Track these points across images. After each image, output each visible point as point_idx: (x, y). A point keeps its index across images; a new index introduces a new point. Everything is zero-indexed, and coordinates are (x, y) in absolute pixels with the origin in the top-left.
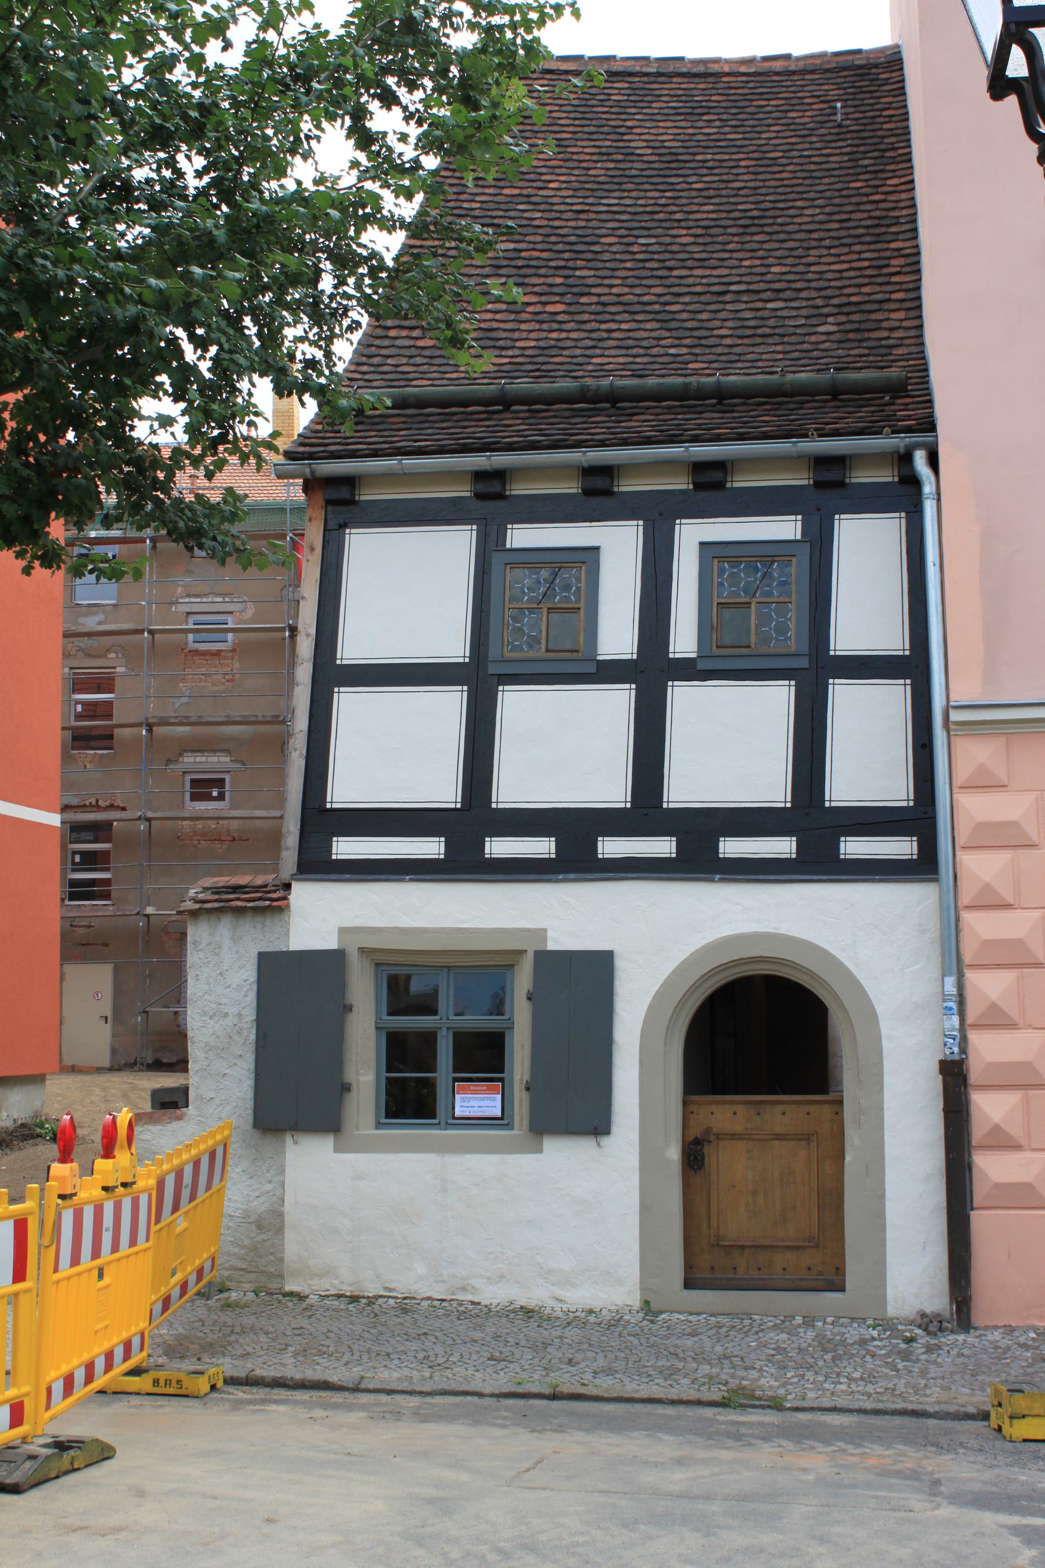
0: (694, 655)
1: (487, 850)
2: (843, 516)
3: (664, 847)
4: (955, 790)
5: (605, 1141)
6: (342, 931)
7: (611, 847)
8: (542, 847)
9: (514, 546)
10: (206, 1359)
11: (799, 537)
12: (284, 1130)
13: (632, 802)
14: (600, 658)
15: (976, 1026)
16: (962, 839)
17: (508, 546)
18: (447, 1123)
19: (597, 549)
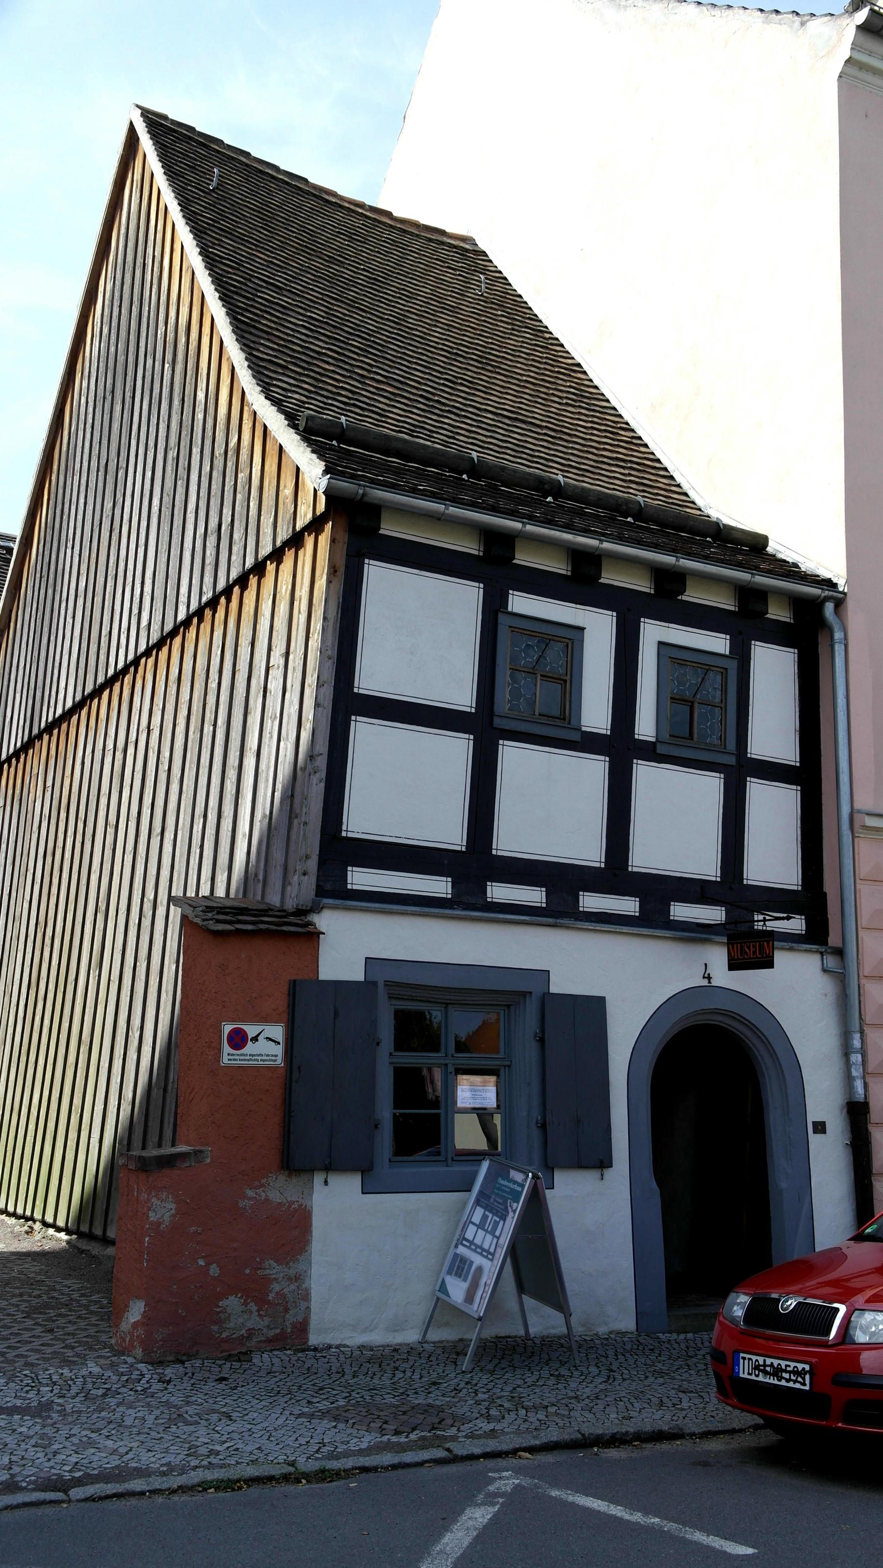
0: (653, 740)
1: (489, 894)
2: (481, 591)
3: (629, 906)
4: (858, 881)
5: (608, 1173)
6: (369, 961)
7: (590, 902)
8: (535, 896)
9: (515, 610)
10: (8, 1477)
11: (727, 653)
12: (311, 1170)
13: (606, 863)
14: (584, 729)
15: (874, 1074)
16: (864, 921)
17: (510, 609)
18: (453, 1160)
19: (583, 629)
